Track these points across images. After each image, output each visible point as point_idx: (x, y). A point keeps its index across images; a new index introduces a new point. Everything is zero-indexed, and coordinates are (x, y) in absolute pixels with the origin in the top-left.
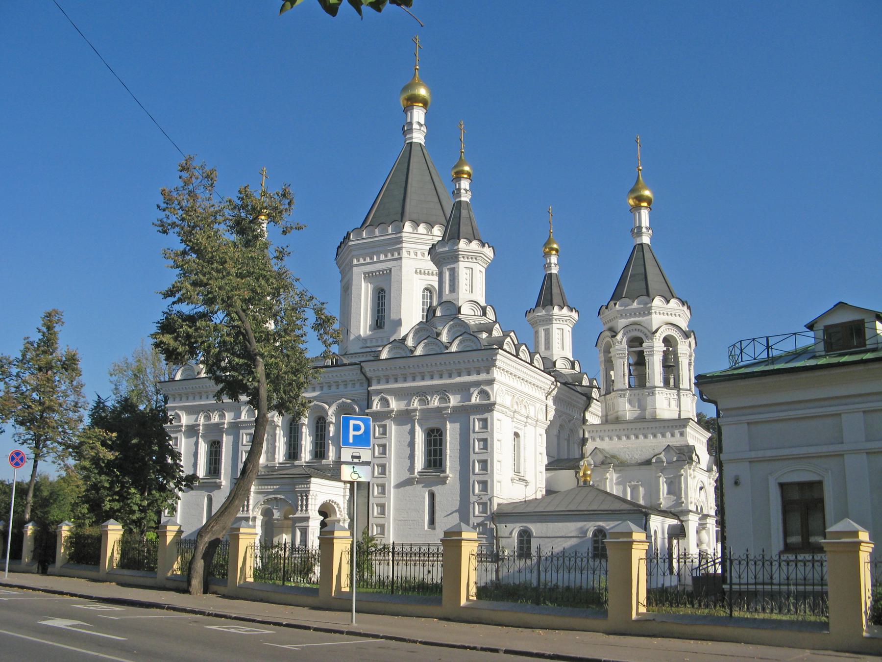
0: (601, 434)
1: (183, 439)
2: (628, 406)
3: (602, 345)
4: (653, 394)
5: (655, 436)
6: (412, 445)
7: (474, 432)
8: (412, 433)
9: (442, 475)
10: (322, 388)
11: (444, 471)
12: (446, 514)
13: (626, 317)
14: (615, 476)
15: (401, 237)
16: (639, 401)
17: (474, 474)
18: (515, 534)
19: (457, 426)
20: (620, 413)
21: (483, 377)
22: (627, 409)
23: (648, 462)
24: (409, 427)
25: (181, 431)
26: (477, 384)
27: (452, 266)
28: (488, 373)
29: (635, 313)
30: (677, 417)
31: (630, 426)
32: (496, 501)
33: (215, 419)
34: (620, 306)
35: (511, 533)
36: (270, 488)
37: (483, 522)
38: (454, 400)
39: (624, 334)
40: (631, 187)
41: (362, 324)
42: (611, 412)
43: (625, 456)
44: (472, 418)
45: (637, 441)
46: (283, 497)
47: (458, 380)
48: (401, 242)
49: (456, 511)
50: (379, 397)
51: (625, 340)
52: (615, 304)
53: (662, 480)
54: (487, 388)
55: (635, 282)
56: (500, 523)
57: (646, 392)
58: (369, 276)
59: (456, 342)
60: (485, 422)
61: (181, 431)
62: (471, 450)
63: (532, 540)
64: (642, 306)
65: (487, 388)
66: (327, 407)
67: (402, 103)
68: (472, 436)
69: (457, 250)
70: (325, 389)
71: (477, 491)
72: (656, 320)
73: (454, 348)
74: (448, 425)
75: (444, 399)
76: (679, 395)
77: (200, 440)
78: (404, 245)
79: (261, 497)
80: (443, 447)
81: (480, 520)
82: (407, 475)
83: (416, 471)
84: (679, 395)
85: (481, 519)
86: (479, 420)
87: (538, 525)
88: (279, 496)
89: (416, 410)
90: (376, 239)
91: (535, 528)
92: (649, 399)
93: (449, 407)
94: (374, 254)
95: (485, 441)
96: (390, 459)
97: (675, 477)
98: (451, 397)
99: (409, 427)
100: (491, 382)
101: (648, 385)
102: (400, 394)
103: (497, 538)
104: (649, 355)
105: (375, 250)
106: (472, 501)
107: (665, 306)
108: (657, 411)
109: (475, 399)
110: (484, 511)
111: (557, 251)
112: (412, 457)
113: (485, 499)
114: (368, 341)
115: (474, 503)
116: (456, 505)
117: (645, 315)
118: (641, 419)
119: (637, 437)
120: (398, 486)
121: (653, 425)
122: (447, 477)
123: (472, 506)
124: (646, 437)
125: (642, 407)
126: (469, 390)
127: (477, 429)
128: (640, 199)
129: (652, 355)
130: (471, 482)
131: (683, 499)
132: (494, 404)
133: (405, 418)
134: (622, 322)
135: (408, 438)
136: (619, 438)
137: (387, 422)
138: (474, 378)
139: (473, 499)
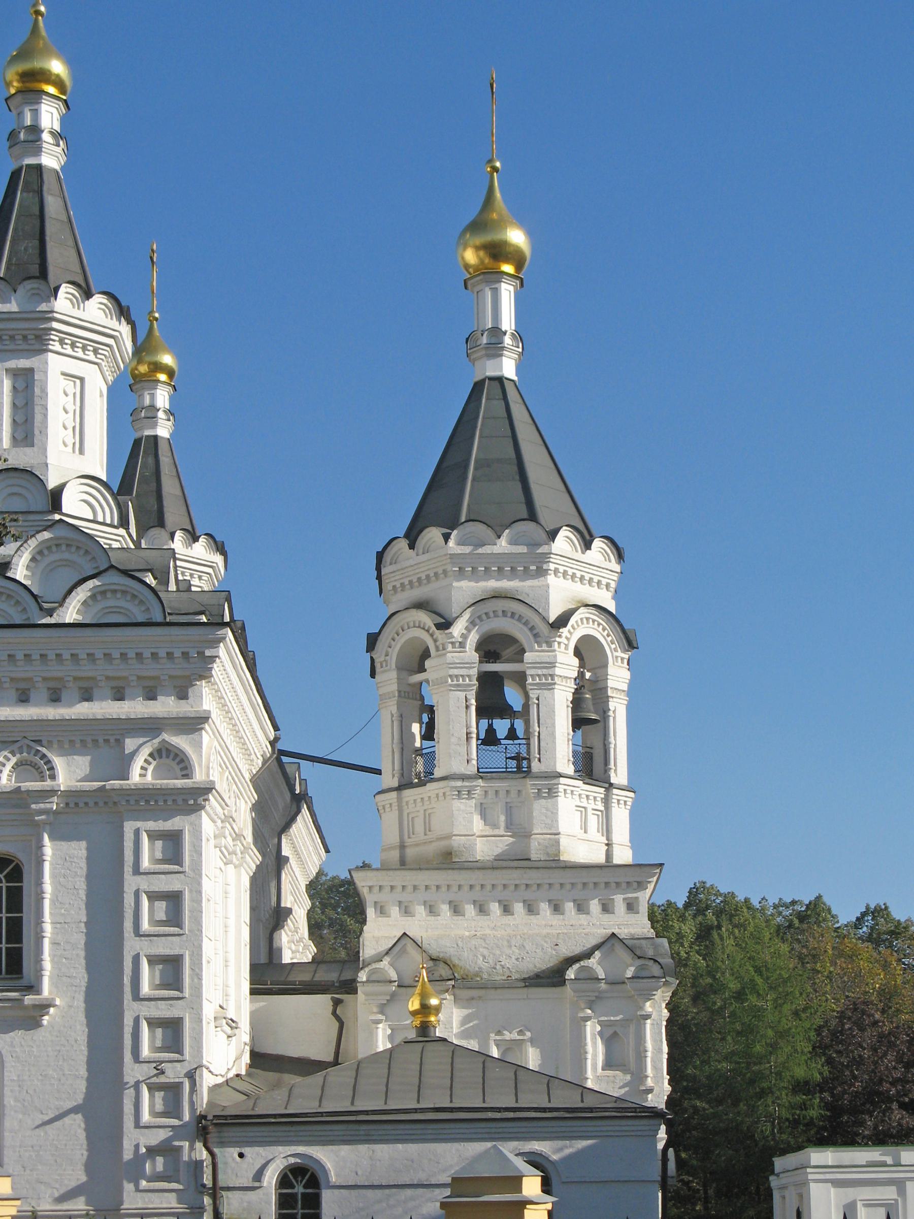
0: (405, 897)
2: (478, 825)
3: (390, 652)
4: (552, 793)
5: (557, 908)
7: (137, 871)
9: (29, 999)
11: (33, 988)
12: (40, 1118)
13: (474, 575)
16: (509, 810)
17: (137, 997)
18: (271, 1178)
19: (79, 850)
20: (457, 842)
21: (165, 706)
22: (472, 828)
23: (552, 977)
26: (149, 727)
27: (23, 363)
28: (183, 695)
30: (601, 859)
31: (490, 878)
32: (208, 1080)
34: (460, 543)
35: (258, 1176)
37: (168, 1140)
38: (69, 772)
39: (472, 623)
40: (471, 214)
42: (420, 835)
43: (473, 959)
44: (129, 827)
45: (508, 919)
47: (83, 710)
49: (74, 1110)
51: (473, 638)
52: (446, 537)
53: (591, 1029)
54: (180, 741)
55: (477, 478)
56: (223, 1144)
57: (530, 786)
59: (81, 594)
60: (173, 844)
62: (128, 925)
63: (327, 1197)
64: (523, 549)
65: (180, 741)
68: (131, 883)
69: (47, 316)
71: (145, 1051)
72: (558, 593)
73: (71, 613)
74: (49, 848)
75: (35, 765)
76: (607, 801)
80: (27, 915)
81: (157, 1137)
84: (607, 801)
86: (153, 836)
87: (345, 1150)
91: (333, 1160)
92: (539, 807)
93: (53, 792)
95: (174, 899)
97: (626, 1022)
98: (59, 762)
100: (195, 724)
101: (536, 766)
103: (215, 1192)
104: (541, 686)
107: (579, 555)
108: (564, 841)
109: (141, 773)
110: (172, 1109)
111: (171, 373)
113: (174, 1073)
115: (137, 1086)
116: (77, 1089)
117: (527, 574)
118: (516, 860)
119: (507, 910)
121: (557, 877)
122: (44, 1007)
123: (129, 1094)
124: (531, 909)
125: (519, 830)
126: (120, 743)
127: (145, 863)
128: (498, 251)
129: (550, 687)
130: (128, 1022)
131: (650, 1082)
132: (206, 790)
134: (464, 590)
136: (456, 910)
138: (135, 708)
139: (132, 1072)
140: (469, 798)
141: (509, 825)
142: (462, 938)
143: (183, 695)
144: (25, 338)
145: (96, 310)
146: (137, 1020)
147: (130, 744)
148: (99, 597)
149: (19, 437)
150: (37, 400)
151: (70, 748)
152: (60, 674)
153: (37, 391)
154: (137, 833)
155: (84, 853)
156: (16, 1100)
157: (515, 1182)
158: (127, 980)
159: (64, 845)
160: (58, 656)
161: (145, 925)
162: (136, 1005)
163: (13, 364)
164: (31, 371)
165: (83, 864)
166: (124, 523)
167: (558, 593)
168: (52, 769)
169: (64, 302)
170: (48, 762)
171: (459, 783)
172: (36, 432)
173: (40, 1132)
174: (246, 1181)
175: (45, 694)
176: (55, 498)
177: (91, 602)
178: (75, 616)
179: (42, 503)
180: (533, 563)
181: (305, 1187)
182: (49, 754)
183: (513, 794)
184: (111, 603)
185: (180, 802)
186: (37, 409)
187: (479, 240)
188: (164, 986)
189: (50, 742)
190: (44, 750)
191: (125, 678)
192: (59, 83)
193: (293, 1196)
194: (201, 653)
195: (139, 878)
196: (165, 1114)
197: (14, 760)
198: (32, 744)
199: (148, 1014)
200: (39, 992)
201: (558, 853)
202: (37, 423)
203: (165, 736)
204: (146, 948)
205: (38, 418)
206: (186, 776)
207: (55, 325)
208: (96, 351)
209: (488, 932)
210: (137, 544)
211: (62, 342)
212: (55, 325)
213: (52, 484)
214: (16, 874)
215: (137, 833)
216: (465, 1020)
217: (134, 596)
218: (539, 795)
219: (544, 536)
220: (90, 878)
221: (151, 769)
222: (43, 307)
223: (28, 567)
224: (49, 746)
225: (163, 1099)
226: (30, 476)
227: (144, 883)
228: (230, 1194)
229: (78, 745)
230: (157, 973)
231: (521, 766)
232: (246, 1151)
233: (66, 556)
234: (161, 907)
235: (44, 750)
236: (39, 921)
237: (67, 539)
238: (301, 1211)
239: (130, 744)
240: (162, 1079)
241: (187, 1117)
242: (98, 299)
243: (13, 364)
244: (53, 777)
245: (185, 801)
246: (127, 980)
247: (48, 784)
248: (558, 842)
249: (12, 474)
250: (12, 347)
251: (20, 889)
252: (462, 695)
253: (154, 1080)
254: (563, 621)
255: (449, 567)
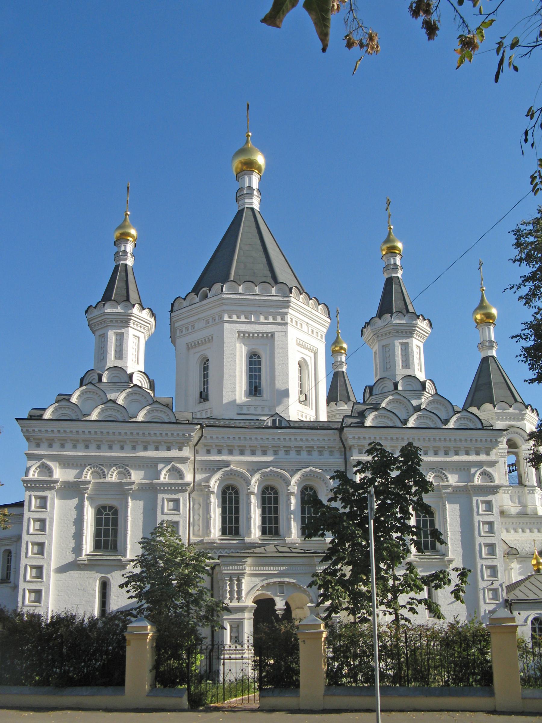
1: (56, 501)
4: (533, 492)
6: (79, 522)
8: (80, 509)
10: (276, 453)
13: (502, 420)
14: (518, 566)
15: (289, 302)
16: (519, 498)
21: (482, 457)
24: (75, 501)
25: (54, 488)
26: (479, 465)
28: (488, 454)
29: (511, 417)
31: (514, 520)
33: (113, 477)
35: (526, 621)
36: (272, 570)
38: (453, 479)
41: (235, 386)
44: (474, 499)
46: (292, 581)
47: (456, 458)
48: (288, 307)
50: (169, 467)
54: (179, 466)
58: (244, 336)
61: (54, 488)
64: (518, 412)
65: (489, 470)
66: (287, 474)
67: (236, 164)
69: (130, 315)
70: (281, 453)
77: (86, 503)
78: (290, 311)
79: (257, 580)
82: (71, 558)
83: (84, 553)
85: (493, 606)
86: (37, 497)
88: (287, 580)
89: (89, 483)
90: (238, 296)
92: (529, 497)
94: (251, 313)
96: (51, 535)
98: (133, 472)
99: (75, 501)
102: (66, 463)
105: (243, 308)
106: (481, 587)
109: (164, 477)
112: (78, 536)
114: (245, 408)
117: (518, 420)
119: (523, 531)
120: (62, 570)
126: (156, 466)
133: (73, 490)
135: (74, 514)
137: (48, 494)
138: (473, 458)
140: (508, 493)
141: (519, 503)
142: (511, 540)
143: (488, 454)
144: (406, 332)
145: (145, 314)
146: (482, 566)
147: (160, 466)
148: (151, 412)
149: (117, 356)
150: (410, 353)
151: (452, 472)
152: (449, 446)
153: (410, 350)
154: (163, 499)
155: (458, 508)
156: (442, 594)
157: (319, 625)
158: (477, 552)
159: (452, 505)
160: (476, 440)
161: (31, 531)
162: (481, 561)
163: (401, 341)
164: (407, 343)
165: (459, 512)
168: (447, 478)
169: (136, 310)
170: (446, 476)
171: (505, 488)
172: (411, 364)
173: (451, 605)
174: (523, 623)
175: (443, 452)
176: (131, 376)
177: (55, 411)
178: (142, 419)
179: (127, 379)
180: (520, 416)
181: (539, 625)
182: (446, 473)
183: (520, 492)
184: (463, 422)
185: (491, 490)
186: (410, 356)
187: (482, 312)
188: (489, 554)
189: (446, 469)
190: (444, 472)
191: (470, 448)
192: (132, 236)
193: (535, 628)
194: (496, 440)
195: (479, 517)
196: (493, 599)
197: (434, 475)
198: (440, 470)
199: (30, 564)
200: (448, 556)
201: (537, 513)
202: (411, 361)
203: (43, 460)
204: (484, 541)
205: (411, 359)
206: (491, 482)
208: (144, 328)
209: (519, 538)
211: (134, 323)
212: (417, 329)
214: (116, 512)
215: (163, 499)
216: (520, 568)
217: (471, 420)
218: (529, 493)
219: (524, 407)
220: (461, 516)
221: (480, 479)
222: (414, 322)
223: (77, 399)
224: (445, 470)
225: (492, 594)
226: (121, 370)
227: (481, 518)
229: (71, 465)
230: (486, 550)
231: (521, 483)
232: (521, 612)
233: (436, 406)
234: (38, 525)
235: (444, 472)
236: (126, 530)
237: (400, 400)
239: (473, 470)
240: (492, 587)
241: (501, 600)
242: (147, 310)
243: (401, 341)
244: (448, 481)
245: (493, 490)
246: (477, 552)
247: (446, 483)
248: (537, 509)
249: (409, 377)
250: (116, 325)
252: (503, 459)
253: (489, 587)
255: (494, 417)
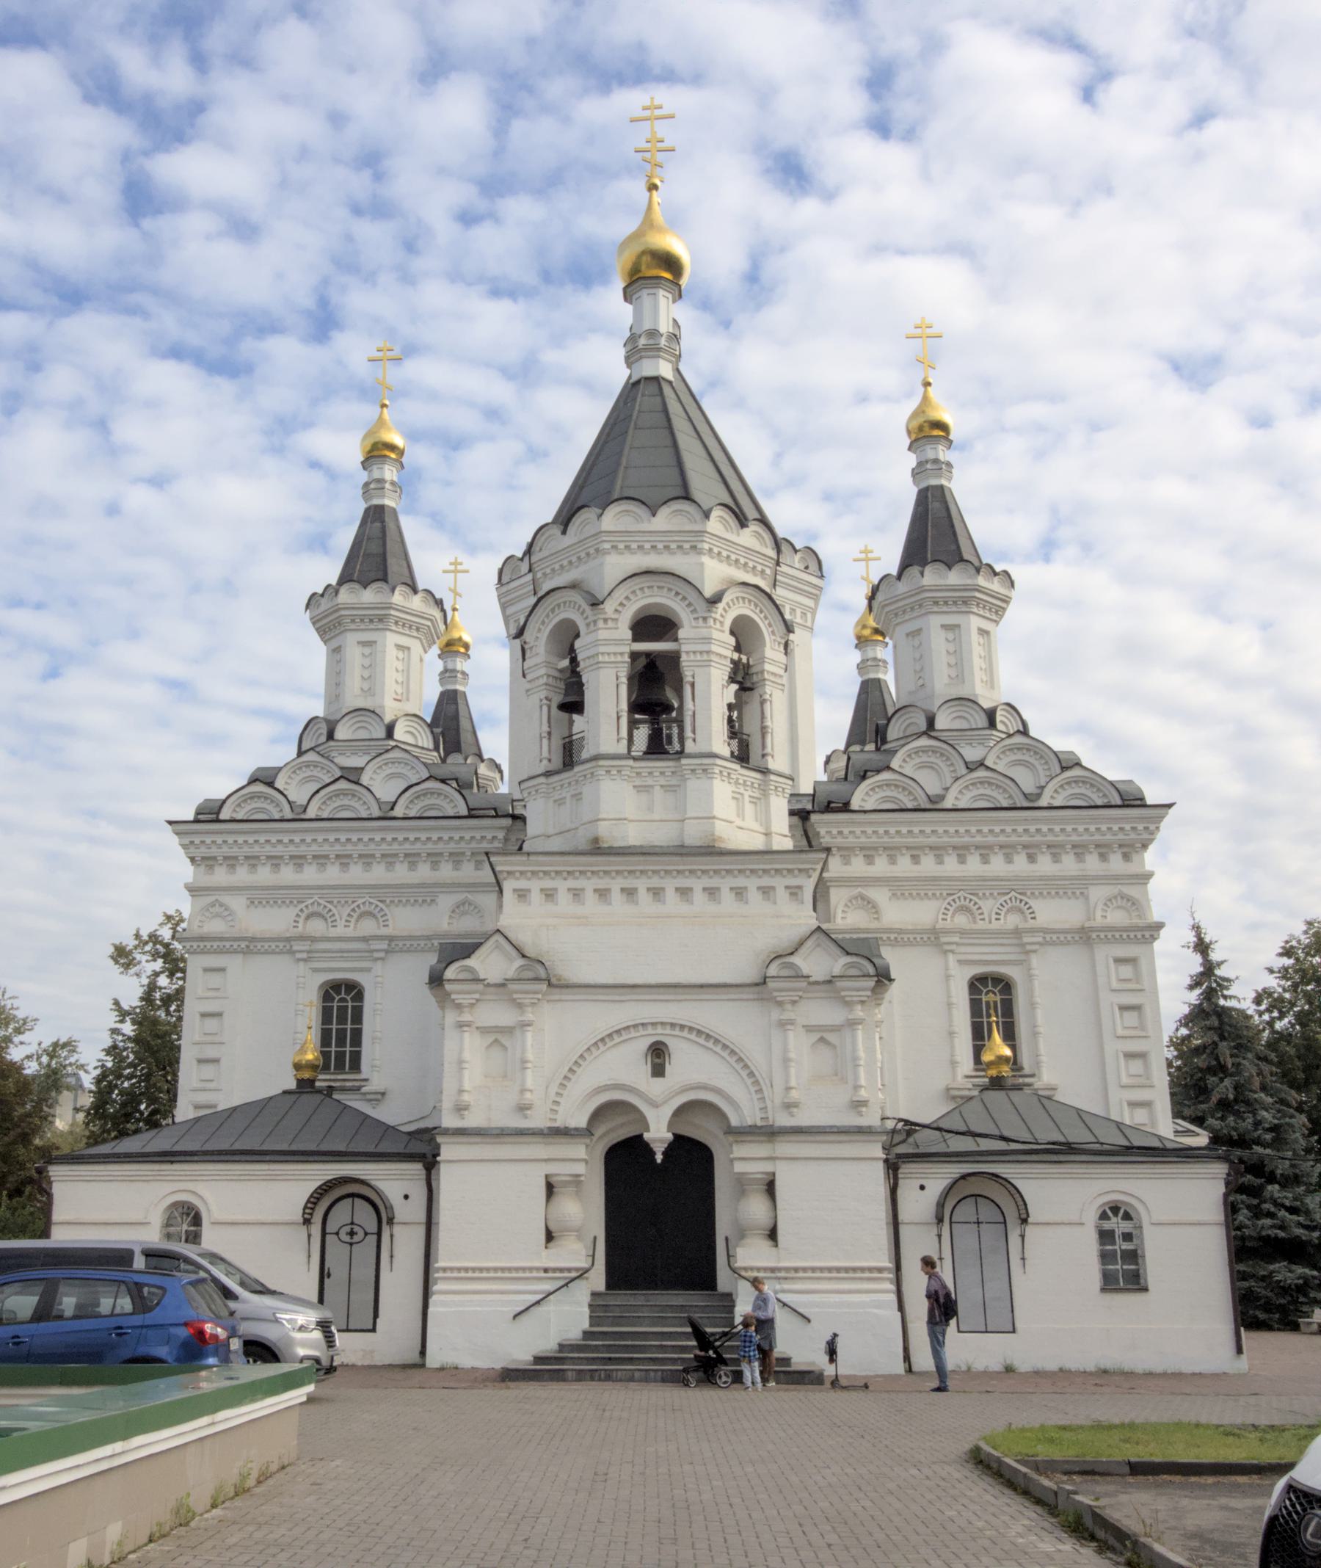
101: (690, 747)
129: (707, 664)
166: (436, 748)
167: (712, 573)
179: (381, 733)
207: (393, 612)
210: (444, 761)
213: (388, 718)
228: (287, 1218)
238: (1117, 1247)
251: (361, 1007)
254: (715, 600)
